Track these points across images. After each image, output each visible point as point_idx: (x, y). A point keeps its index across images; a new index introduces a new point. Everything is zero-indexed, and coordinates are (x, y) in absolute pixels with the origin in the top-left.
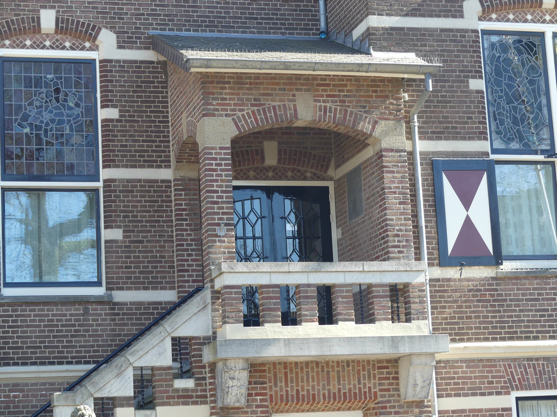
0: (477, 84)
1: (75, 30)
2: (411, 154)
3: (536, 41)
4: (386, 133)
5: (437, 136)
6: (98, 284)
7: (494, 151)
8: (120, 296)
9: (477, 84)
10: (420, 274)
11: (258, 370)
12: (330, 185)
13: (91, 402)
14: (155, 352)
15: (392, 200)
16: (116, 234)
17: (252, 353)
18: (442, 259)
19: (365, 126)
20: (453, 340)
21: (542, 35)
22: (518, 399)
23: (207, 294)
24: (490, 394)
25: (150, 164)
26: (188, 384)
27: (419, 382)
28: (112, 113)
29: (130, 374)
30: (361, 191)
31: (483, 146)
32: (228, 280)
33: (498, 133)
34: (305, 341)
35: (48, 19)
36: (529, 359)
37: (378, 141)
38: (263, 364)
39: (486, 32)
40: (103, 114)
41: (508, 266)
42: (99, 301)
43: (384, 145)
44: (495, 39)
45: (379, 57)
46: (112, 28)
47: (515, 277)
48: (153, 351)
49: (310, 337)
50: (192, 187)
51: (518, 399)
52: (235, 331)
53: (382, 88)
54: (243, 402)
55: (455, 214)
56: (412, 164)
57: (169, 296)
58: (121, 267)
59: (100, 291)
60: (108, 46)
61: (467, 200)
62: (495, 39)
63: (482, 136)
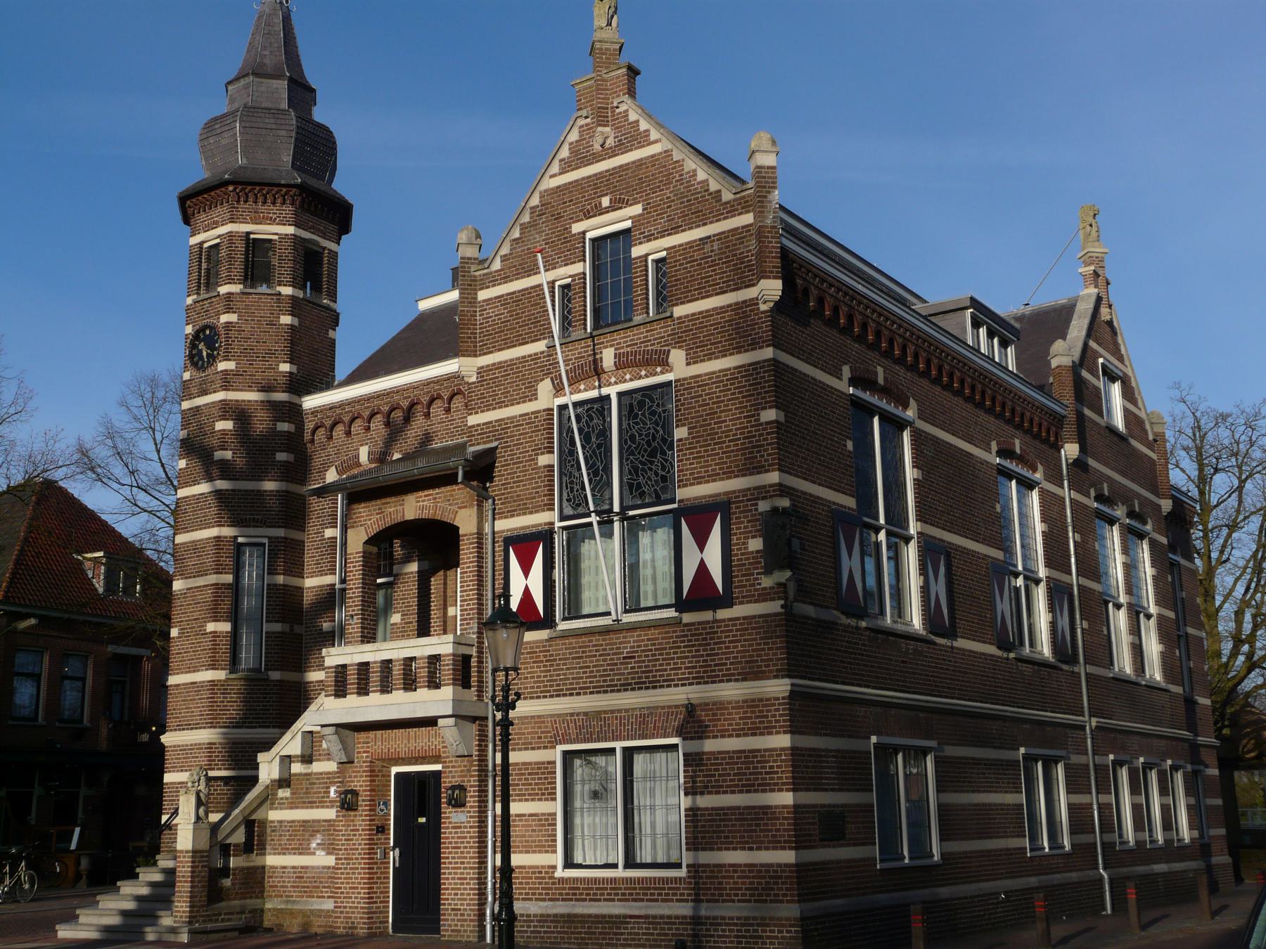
21: (608, 397)
24: (539, 748)
36: (572, 715)
55: (713, 555)
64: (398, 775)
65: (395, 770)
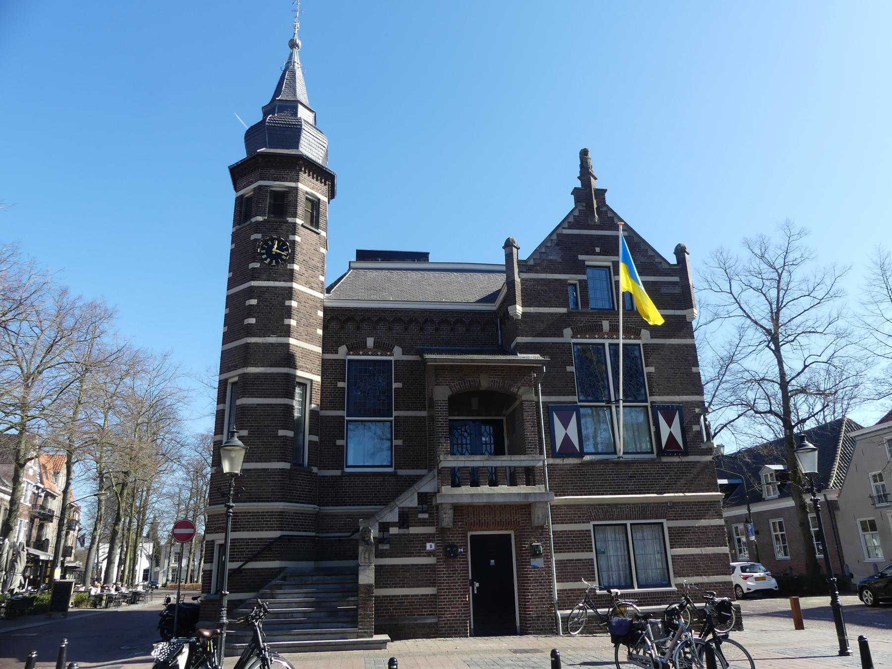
0: (571, 369)
1: (383, 347)
2: (538, 403)
3: (601, 347)
6: (390, 466)
7: (580, 401)
8: (401, 472)
9: (571, 369)
10: (543, 461)
11: (459, 509)
12: (504, 418)
13: (377, 524)
14: (410, 500)
15: (528, 425)
16: (399, 442)
17: (455, 501)
18: (553, 454)
20: (556, 495)
21: (603, 345)
22: (594, 525)
26: (426, 516)
27: (541, 516)
29: (397, 510)
30: (516, 420)
31: (575, 398)
32: (443, 464)
33: (582, 392)
34: (480, 495)
35: (370, 342)
36: (600, 505)
37: (521, 397)
38: (462, 506)
39: (574, 344)
40: (394, 385)
41: (587, 458)
43: (523, 398)
45: (520, 356)
46: (400, 346)
50: (432, 418)
51: (594, 525)
52: (446, 489)
53: (526, 369)
56: (538, 408)
58: (401, 457)
59: (391, 470)
60: (398, 354)
61: (566, 425)
63: (573, 394)
64: (472, 536)
65: (470, 534)
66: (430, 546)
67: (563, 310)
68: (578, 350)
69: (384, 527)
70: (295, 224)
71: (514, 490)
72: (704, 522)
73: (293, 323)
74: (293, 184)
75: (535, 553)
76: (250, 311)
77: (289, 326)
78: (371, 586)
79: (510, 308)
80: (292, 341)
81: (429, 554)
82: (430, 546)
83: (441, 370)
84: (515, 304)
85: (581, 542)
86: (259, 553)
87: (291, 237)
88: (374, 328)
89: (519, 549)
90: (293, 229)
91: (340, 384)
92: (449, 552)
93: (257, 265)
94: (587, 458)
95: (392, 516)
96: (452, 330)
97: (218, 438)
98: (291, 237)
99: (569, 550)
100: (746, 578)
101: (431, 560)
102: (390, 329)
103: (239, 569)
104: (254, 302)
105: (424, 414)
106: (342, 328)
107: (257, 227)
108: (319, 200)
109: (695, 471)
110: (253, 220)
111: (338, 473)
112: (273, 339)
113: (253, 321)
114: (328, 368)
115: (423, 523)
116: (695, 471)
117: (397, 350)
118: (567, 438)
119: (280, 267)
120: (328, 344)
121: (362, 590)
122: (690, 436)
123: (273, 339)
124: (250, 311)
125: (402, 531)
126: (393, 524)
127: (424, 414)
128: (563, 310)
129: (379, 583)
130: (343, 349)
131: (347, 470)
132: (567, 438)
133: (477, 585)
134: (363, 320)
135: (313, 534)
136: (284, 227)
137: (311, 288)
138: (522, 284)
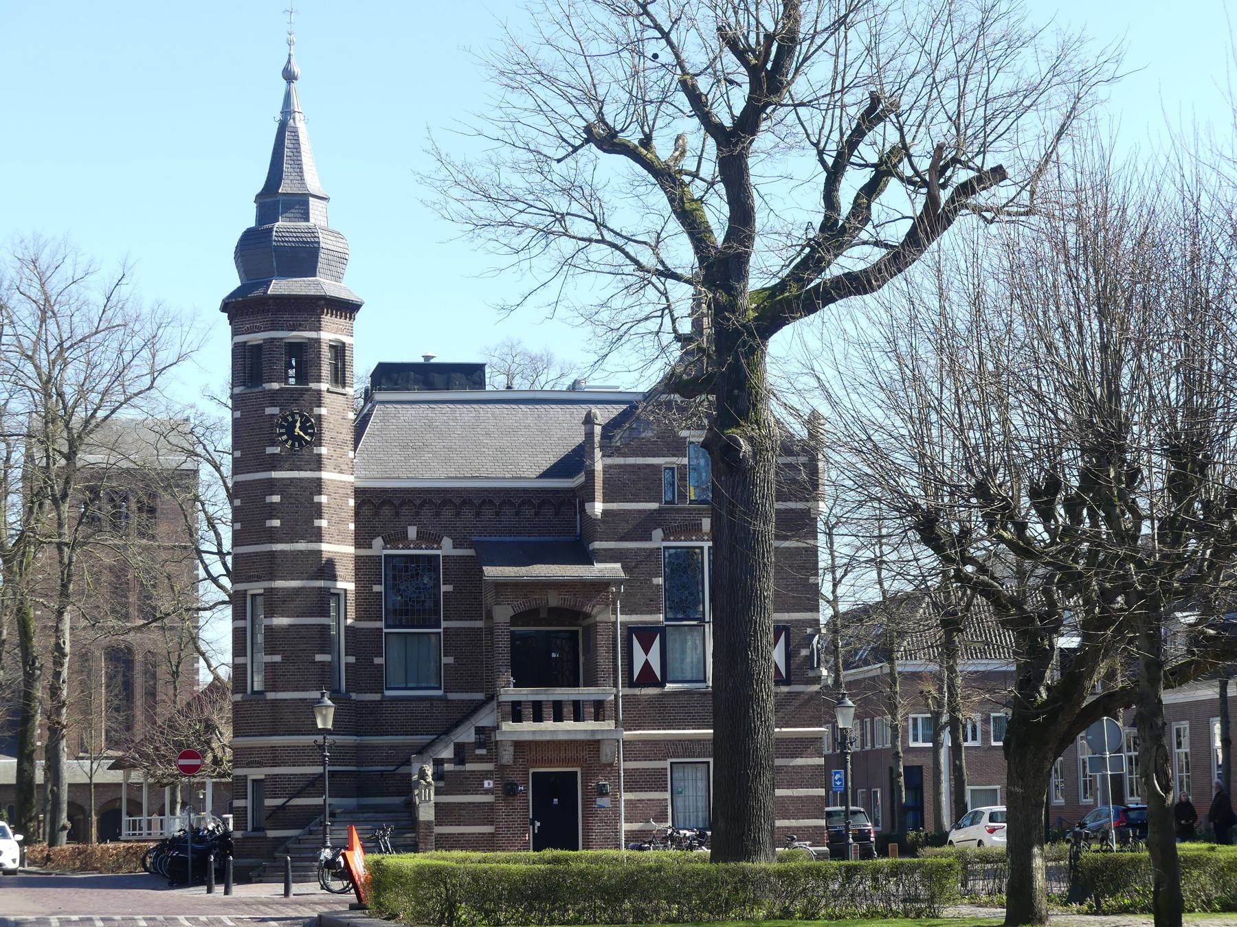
1: (429, 538)
2: (615, 623)
4: (599, 613)
5: (632, 612)
6: (439, 688)
11: (519, 745)
14: (466, 735)
17: (515, 738)
18: (630, 683)
19: (588, 609)
23: (494, 703)
25: (471, 618)
26: (484, 752)
28: (449, 588)
35: (412, 532)
39: (665, 548)
40: (443, 588)
41: (670, 687)
42: (439, 698)
43: (598, 619)
44: (672, 551)
47: (674, 694)
48: (619, 257)
49: (548, 728)
50: (490, 631)
52: (508, 726)
53: (600, 586)
54: (511, 762)
55: (639, 658)
57: (480, 696)
59: (439, 693)
60: (446, 548)
62: (672, 551)
64: (534, 774)
65: (531, 771)
66: (487, 784)
67: (654, 506)
68: (670, 555)
69: (438, 763)
70: (319, 392)
71: (580, 726)
72: (799, 761)
73: (324, 523)
74: (313, 335)
75: (602, 792)
76: (272, 511)
77: (320, 528)
78: (430, 822)
79: (587, 505)
80: (325, 547)
81: (487, 792)
82: (487, 784)
83: (501, 586)
84: (593, 501)
85: (654, 781)
86: (304, 789)
87: (316, 411)
88: (417, 514)
89: (585, 786)
90: (318, 399)
91: (376, 588)
92: (509, 790)
93: (277, 450)
94: (670, 687)
95: (447, 753)
96: (517, 514)
97: (240, 660)
98: (316, 411)
99: (641, 789)
100: (992, 831)
101: (489, 798)
102: (438, 514)
103: (283, 807)
104: (276, 499)
105: (479, 624)
106: (377, 514)
107: (274, 398)
108: (344, 344)
109: (796, 703)
110: (267, 386)
111: (377, 697)
112: (302, 546)
113: (276, 523)
114: (365, 569)
115: (481, 759)
116: (796, 703)
117: (447, 543)
118: (647, 665)
119: (305, 451)
120: (361, 539)
121: (422, 826)
122: (796, 661)
123: (302, 546)
124: (272, 511)
125: (458, 768)
126: (449, 761)
127: (479, 624)
128: (654, 506)
129: (440, 821)
130: (378, 542)
131: (388, 693)
132: (647, 665)
133: (538, 824)
134: (403, 503)
135: (354, 768)
136: (306, 397)
137: (341, 472)
138: (604, 472)
